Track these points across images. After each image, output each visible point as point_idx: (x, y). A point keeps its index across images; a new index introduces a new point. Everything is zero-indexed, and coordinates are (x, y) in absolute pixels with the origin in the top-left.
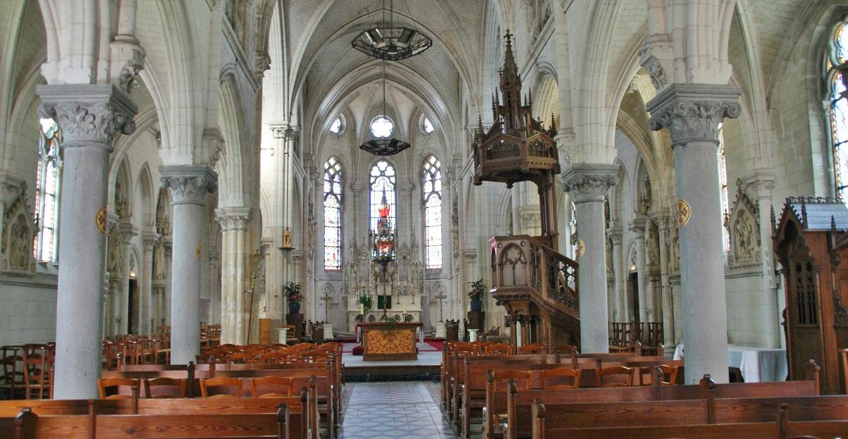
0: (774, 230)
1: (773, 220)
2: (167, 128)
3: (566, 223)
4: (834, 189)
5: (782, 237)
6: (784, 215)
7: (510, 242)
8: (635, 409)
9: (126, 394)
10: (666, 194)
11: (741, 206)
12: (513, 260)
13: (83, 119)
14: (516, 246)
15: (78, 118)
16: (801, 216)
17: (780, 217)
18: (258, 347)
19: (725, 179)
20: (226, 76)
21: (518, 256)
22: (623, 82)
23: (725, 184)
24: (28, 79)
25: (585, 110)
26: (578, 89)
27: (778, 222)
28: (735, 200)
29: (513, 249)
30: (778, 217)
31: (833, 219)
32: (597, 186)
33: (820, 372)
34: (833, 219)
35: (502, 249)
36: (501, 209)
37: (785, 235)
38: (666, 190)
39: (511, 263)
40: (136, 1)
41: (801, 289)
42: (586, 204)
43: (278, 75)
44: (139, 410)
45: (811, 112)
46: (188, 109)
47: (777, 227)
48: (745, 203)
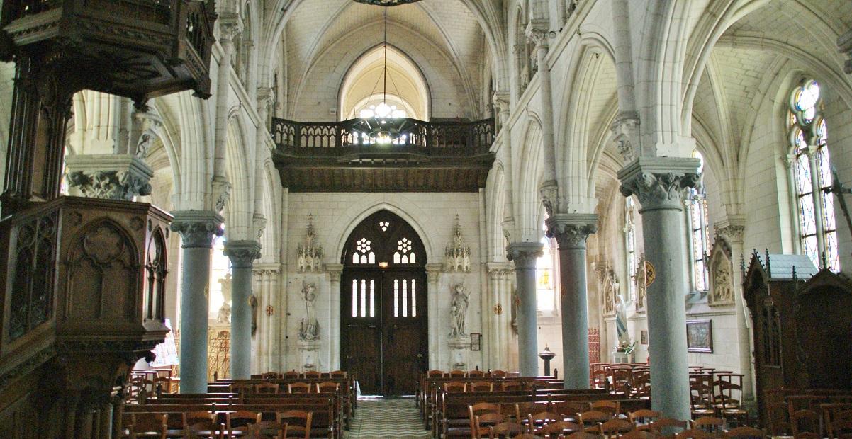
0: (744, 276)
1: (742, 268)
4: (797, 237)
5: (750, 285)
6: (752, 264)
9: (268, 261)
11: (719, 248)
13: (107, 186)
15: (102, 184)
16: (764, 263)
17: (749, 265)
20: (233, 117)
23: (707, 224)
24: (261, 322)
26: (644, 58)
27: (747, 270)
28: (714, 242)
30: (747, 265)
31: (794, 269)
33: (371, 163)
34: (794, 269)
37: (753, 283)
40: (626, 4)
41: (776, 333)
45: (789, 75)
46: (198, 160)
47: (746, 274)
48: (720, 248)
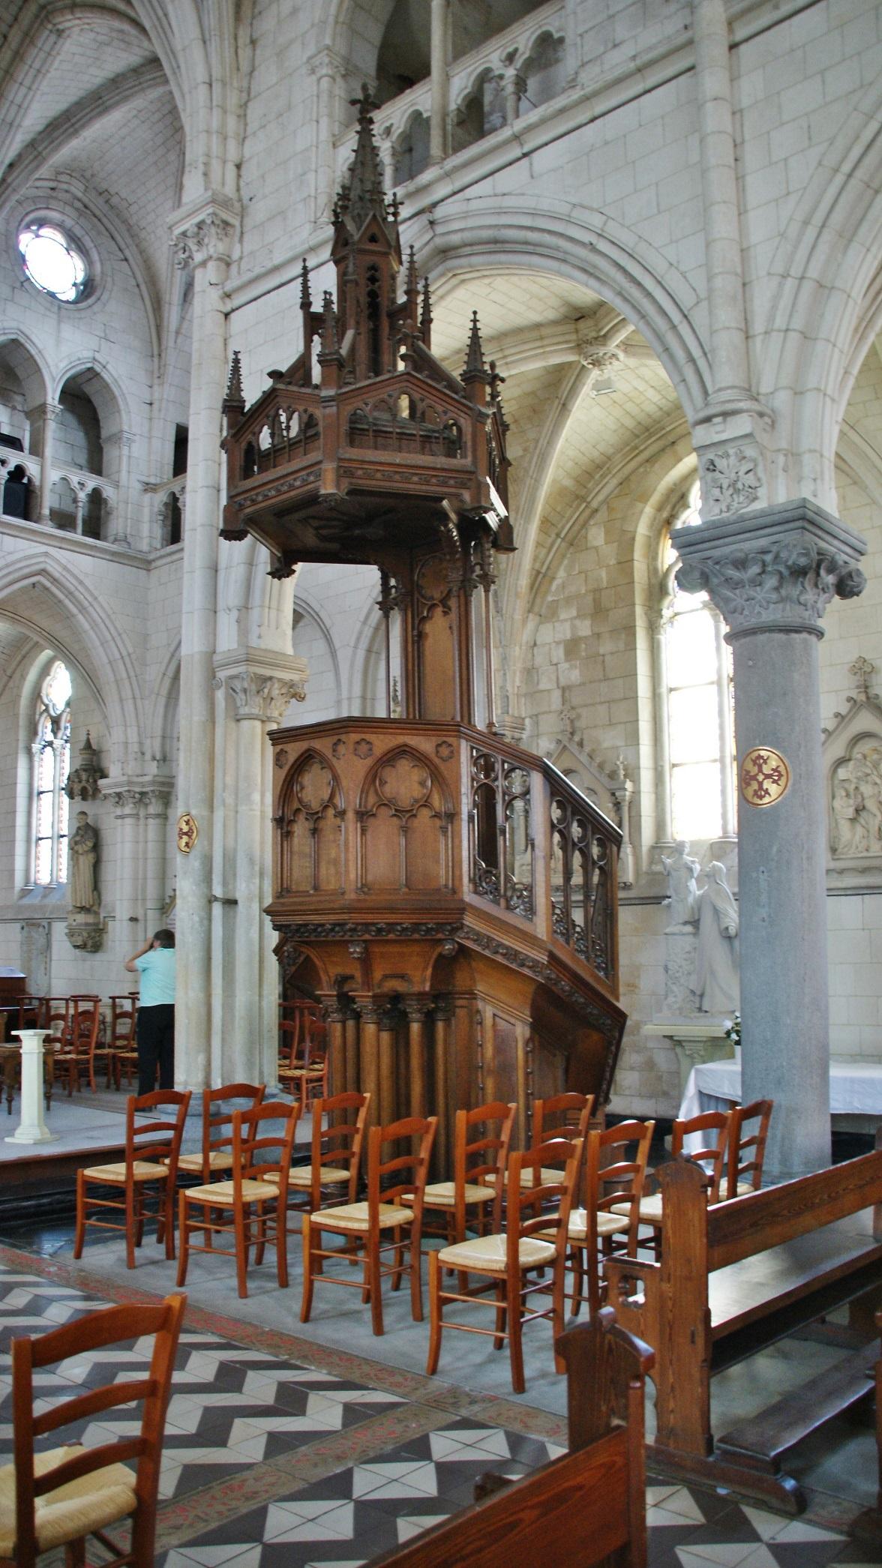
2: (173, 53)
3: (21, 745)
7: (401, 739)
8: (579, 1479)
10: (518, 683)
12: (315, 806)
14: (420, 759)
18: (48, 1008)
19: (731, 667)
21: (417, 792)
22: (525, 358)
25: (820, 346)
29: (404, 765)
32: (756, 582)
35: (287, 768)
36: (124, 645)
38: (518, 674)
39: (399, 813)
42: (794, 636)
43: (14, 109)
44: (527, 1385)
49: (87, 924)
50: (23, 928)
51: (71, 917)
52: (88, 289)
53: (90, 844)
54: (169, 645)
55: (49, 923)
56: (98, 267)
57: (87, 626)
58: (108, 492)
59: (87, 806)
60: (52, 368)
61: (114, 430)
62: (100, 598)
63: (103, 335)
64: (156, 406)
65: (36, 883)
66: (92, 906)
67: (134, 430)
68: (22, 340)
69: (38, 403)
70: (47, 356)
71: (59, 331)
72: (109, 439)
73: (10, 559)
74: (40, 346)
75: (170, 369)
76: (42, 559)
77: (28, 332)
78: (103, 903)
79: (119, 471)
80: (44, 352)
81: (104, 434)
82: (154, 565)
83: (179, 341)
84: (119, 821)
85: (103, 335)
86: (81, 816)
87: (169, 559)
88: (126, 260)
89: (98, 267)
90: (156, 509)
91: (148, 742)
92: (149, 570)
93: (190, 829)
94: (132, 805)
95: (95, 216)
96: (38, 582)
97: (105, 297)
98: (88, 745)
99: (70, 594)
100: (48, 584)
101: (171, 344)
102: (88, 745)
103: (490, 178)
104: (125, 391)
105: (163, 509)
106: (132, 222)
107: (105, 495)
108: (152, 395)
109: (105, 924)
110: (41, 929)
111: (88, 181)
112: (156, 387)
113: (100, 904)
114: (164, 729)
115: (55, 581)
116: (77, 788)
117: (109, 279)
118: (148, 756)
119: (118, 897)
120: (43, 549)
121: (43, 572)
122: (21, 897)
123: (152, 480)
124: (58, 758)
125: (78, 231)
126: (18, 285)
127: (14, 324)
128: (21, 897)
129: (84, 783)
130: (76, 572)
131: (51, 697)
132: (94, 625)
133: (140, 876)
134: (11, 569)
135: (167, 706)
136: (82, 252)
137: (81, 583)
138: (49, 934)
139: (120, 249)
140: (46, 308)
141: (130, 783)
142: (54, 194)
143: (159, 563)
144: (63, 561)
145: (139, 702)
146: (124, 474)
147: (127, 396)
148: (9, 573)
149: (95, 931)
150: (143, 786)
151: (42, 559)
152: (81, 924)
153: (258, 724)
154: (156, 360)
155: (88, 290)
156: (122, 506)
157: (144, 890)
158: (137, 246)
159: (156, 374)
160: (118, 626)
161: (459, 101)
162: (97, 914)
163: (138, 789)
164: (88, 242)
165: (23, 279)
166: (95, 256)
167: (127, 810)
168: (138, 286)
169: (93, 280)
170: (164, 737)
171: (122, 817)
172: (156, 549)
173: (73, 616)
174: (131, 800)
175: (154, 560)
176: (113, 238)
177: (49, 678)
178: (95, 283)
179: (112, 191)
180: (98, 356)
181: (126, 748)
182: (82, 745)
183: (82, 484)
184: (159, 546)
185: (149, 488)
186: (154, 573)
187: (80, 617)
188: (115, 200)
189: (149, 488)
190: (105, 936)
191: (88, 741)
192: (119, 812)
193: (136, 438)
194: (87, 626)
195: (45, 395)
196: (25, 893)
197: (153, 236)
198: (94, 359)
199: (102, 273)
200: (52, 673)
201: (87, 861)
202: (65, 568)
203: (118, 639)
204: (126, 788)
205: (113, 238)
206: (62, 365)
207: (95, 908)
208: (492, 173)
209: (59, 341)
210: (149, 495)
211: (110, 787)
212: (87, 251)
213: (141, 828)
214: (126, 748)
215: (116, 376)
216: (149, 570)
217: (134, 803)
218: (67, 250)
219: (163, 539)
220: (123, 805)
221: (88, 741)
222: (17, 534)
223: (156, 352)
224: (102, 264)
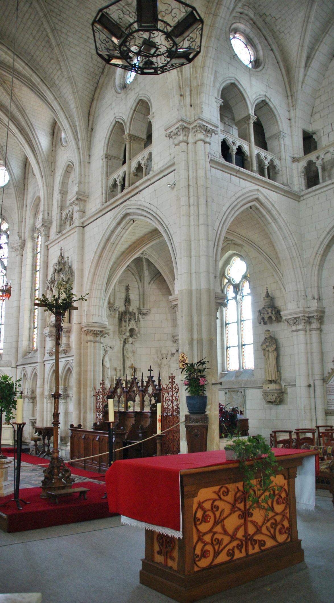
49: (276, 390)
50: (226, 393)
51: (265, 387)
52: (257, 63)
53: (275, 347)
54: (319, 238)
55: (244, 390)
56: (261, 53)
57: (276, 229)
58: (277, 162)
59: (268, 327)
60: (250, 98)
61: (274, 131)
62: (282, 214)
63: (267, 85)
64: (293, 120)
65: (227, 370)
66: (277, 380)
67: (285, 132)
68: (237, 83)
69: (246, 115)
70: (247, 92)
71: (251, 81)
72: (271, 137)
73: (244, 191)
74: (245, 88)
75: (299, 101)
76: (256, 193)
77: (239, 80)
78: (282, 378)
79: (280, 152)
80: (246, 90)
81: (267, 135)
82: (302, 198)
83: (303, 86)
84: (295, 333)
85: (267, 85)
86: (267, 332)
87: (314, 194)
88: (272, 50)
89: (261, 53)
90: (300, 170)
91: (309, 290)
92: (299, 201)
93: (184, 359)
94: (303, 324)
95: (258, 28)
96: (254, 205)
97: (266, 66)
98: (268, 295)
99: (269, 211)
100: (258, 206)
101: (300, 88)
102: (268, 295)
103: (153, 185)
104: (279, 113)
105: (304, 170)
106: (275, 30)
107: (275, 164)
108: (290, 115)
109: (286, 389)
110: (239, 393)
111: (256, 9)
112: (292, 111)
113: (281, 380)
114: (318, 283)
115: (261, 204)
116: (266, 317)
117: (266, 58)
118: (310, 297)
119: (297, 374)
120: (257, 187)
121: (257, 199)
122: (221, 378)
123: (296, 156)
124: (239, 305)
125: (251, 35)
126: (233, 57)
127: (233, 75)
128: (221, 378)
129: (270, 314)
130: (271, 200)
131: (230, 275)
132: (280, 228)
133: (310, 361)
134: (244, 197)
135: (319, 270)
136: (252, 46)
137: (273, 206)
138: (244, 396)
139: (269, 45)
140: (244, 69)
141: (304, 312)
142: (242, 16)
143: (305, 197)
144: (266, 194)
145: (302, 268)
146: (283, 153)
147: (280, 115)
148: (244, 199)
149: (280, 393)
150: (309, 314)
151: (256, 193)
152: (273, 390)
153: (92, 343)
154: (290, 98)
155: (257, 64)
156: (284, 169)
157: (312, 369)
158: (277, 43)
159: (291, 105)
160: (290, 229)
161: (110, 185)
162: (280, 384)
163: (307, 315)
164: (256, 41)
165: (234, 54)
166: (259, 47)
167: (300, 327)
168: (278, 63)
169: (259, 60)
170: (318, 287)
171: (297, 331)
172: (302, 190)
173: (269, 223)
174: (304, 321)
175: (303, 196)
176: (266, 39)
177: (229, 266)
178: (260, 61)
179: (267, 14)
180: (267, 94)
181: (298, 294)
182: (264, 295)
183: (266, 158)
184: (304, 188)
185: (295, 160)
186: (303, 203)
187: (273, 224)
188: (268, 19)
189: (295, 160)
190: (285, 396)
191: (267, 293)
192: (294, 328)
193: (286, 135)
194: (276, 229)
195: (248, 110)
196: (223, 375)
197: (288, 35)
198: (265, 96)
199: (263, 55)
200: (231, 263)
201: (272, 357)
202: (266, 198)
203: (290, 236)
204: (302, 315)
205: (266, 39)
206: (254, 97)
207: (279, 381)
208: (148, 186)
209: (251, 86)
210: (296, 163)
211: (289, 314)
212: (255, 46)
213: (308, 336)
214: (298, 294)
215: (275, 105)
216: (299, 201)
217: (304, 323)
218: (246, 45)
219: (306, 186)
220: (298, 324)
221: (267, 293)
222: (245, 178)
223: (289, 94)
224: (263, 51)
